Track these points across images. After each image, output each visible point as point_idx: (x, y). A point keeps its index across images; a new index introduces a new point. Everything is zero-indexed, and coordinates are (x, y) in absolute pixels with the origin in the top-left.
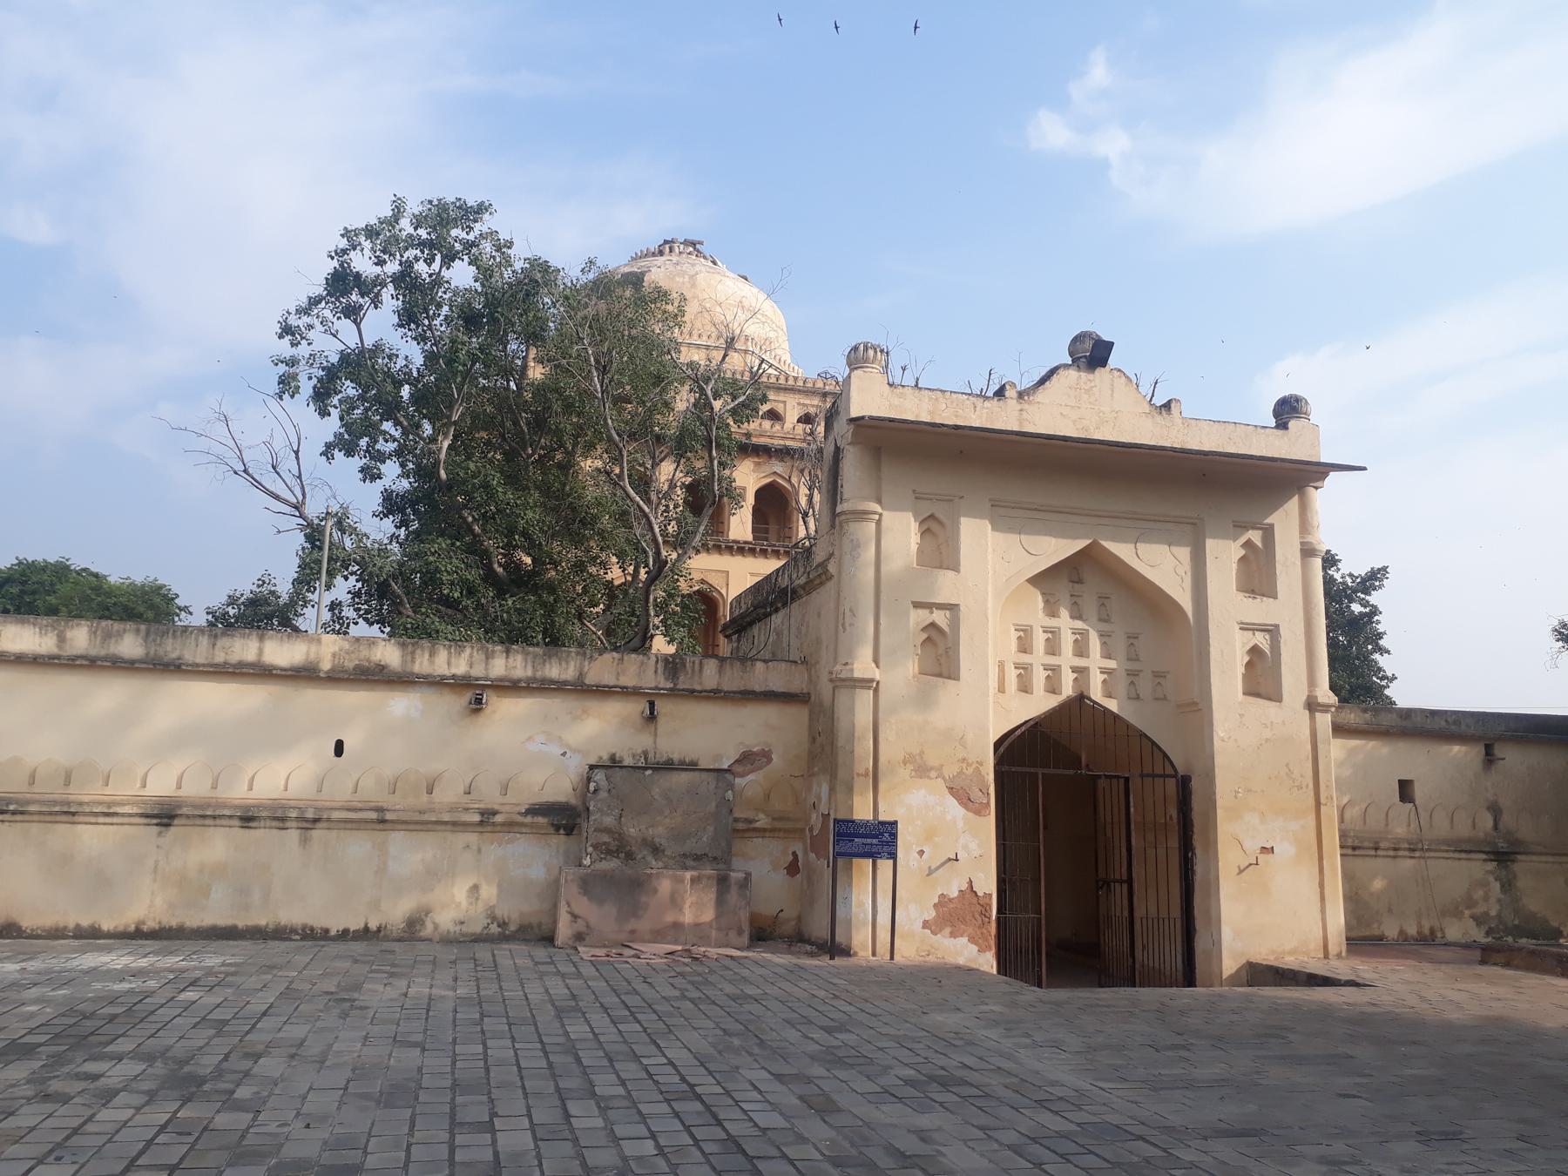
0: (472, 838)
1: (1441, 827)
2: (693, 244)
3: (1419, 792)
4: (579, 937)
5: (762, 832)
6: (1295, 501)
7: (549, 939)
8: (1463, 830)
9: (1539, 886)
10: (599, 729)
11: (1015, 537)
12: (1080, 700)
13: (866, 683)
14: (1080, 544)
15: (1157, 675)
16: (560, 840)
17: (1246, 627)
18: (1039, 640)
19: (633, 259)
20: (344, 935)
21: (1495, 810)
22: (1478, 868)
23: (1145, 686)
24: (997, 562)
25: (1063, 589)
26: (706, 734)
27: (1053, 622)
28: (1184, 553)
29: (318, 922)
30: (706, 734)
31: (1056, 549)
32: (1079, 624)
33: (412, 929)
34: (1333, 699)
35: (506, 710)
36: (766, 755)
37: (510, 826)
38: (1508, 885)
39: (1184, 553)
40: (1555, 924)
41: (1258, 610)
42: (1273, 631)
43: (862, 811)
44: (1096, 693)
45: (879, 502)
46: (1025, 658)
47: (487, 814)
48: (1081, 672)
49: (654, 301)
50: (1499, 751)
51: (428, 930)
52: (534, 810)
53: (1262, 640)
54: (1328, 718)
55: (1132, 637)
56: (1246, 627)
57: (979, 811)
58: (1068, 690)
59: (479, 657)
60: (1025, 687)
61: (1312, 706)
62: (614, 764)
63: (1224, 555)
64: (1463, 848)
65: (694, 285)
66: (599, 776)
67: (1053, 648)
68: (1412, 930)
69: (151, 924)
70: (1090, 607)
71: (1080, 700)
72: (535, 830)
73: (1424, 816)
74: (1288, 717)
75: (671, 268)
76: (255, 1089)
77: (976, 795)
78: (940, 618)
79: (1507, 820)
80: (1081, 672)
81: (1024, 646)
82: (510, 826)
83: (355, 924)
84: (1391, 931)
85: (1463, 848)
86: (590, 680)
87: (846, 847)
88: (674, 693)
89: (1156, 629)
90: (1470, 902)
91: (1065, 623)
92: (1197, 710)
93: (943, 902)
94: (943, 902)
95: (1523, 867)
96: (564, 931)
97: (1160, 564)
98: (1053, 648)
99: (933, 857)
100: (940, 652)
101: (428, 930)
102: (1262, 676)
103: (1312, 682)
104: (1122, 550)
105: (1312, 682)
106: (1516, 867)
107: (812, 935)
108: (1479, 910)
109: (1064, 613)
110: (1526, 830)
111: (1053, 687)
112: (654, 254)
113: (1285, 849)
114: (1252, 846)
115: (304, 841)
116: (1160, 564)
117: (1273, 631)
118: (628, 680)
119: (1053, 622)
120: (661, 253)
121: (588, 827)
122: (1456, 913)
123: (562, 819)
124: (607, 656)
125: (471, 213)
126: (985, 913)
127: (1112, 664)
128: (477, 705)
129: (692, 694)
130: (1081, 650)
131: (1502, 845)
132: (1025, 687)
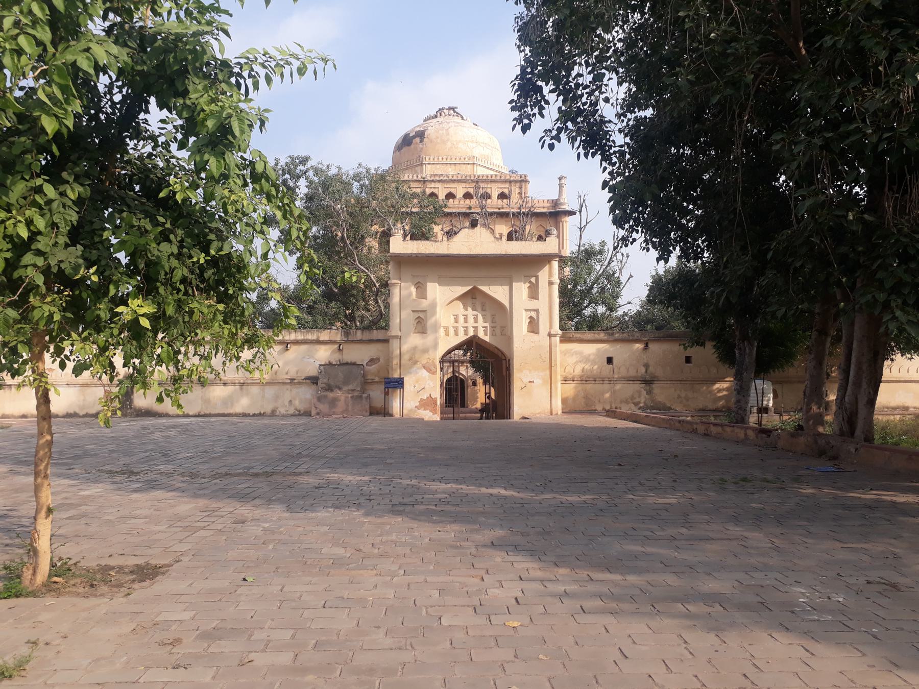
0: (288, 387)
1: (623, 372)
2: (453, 109)
3: (615, 361)
4: (318, 414)
5: (377, 382)
6: (547, 266)
7: (310, 415)
8: (632, 373)
9: (661, 393)
10: (324, 354)
11: (447, 288)
12: (475, 337)
13: (396, 337)
14: (470, 288)
15: (502, 327)
16: (314, 387)
17: (527, 310)
18: (461, 319)
19: (425, 120)
20: (254, 415)
21: (647, 366)
22: (637, 386)
23: (498, 331)
24: (442, 296)
25: (469, 301)
26: (359, 354)
27: (466, 312)
28: (507, 288)
29: (247, 412)
30: (359, 354)
31: (462, 290)
32: (475, 312)
33: (273, 414)
34: (560, 332)
35: (293, 349)
36: (378, 359)
37: (299, 383)
38: (649, 392)
39: (507, 288)
40: (669, 405)
41: (534, 304)
42: (537, 311)
43: (396, 375)
44: (481, 334)
45: (400, 279)
46: (456, 325)
47: (292, 380)
48: (476, 328)
49: (246, 290)
50: (650, 345)
51: (278, 413)
52: (306, 378)
53: (534, 314)
54: (558, 339)
55: (493, 316)
56: (527, 310)
57: (434, 373)
58: (471, 333)
59: (287, 333)
60: (457, 334)
61: (550, 335)
62: (330, 364)
63: (521, 289)
64: (631, 380)
65: (448, 134)
66: (322, 368)
67: (466, 321)
68: (608, 408)
69: (202, 413)
70: (479, 308)
71: (475, 337)
72: (307, 384)
73: (616, 369)
74: (542, 338)
75: (437, 126)
76: (193, 400)
77: (433, 369)
78: (422, 315)
79: (651, 369)
80: (476, 328)
81: (456, 322)
82: (299, 383)
83: (257, 412)
84: (599, 408)
85: (631, 380)
86: (321, 339)
87: (388, 385)
88: (347, 342)
89: (499, 314)
90: (632, 398)
91: (470, 311)
92: (509, 340)
93: (422, 400)
94: (422, 400)
95: (657, 388)
96: (314, 412)
97: (498, 292)
98: (466, 321)
99: (418, 387)
100: (421, 324)
101: (278, 413)
102: (533, 325)
103: (551, 327)
104: (481, 288)
105: (551, 327)
106: (654, 386)
107: (385, 412)
108: (637, 400)
109: (470, 309)
110: (659, 372)
111: (466, 333)
112: (433, 118)
113: (538, 381)
114: (526, 380)
115: (241, 389)
116: (498, 292)
117: (537, 311)
118: (333, 339)
119: (466, 312)
120: (436, 116)
121: (320, 382)
122: (627, 402)
123: (313, 380)
124: (326, 331)
125: (304, 160)
126: (435, 401)
127: (487, 324)
128: (287, 349)
129: (353, 341)
130: (476, 321)
131: (648, 378)
132: (457, 334)
